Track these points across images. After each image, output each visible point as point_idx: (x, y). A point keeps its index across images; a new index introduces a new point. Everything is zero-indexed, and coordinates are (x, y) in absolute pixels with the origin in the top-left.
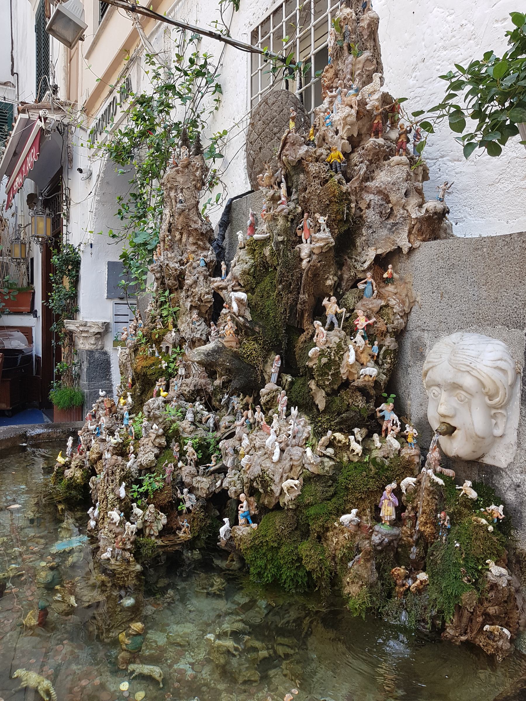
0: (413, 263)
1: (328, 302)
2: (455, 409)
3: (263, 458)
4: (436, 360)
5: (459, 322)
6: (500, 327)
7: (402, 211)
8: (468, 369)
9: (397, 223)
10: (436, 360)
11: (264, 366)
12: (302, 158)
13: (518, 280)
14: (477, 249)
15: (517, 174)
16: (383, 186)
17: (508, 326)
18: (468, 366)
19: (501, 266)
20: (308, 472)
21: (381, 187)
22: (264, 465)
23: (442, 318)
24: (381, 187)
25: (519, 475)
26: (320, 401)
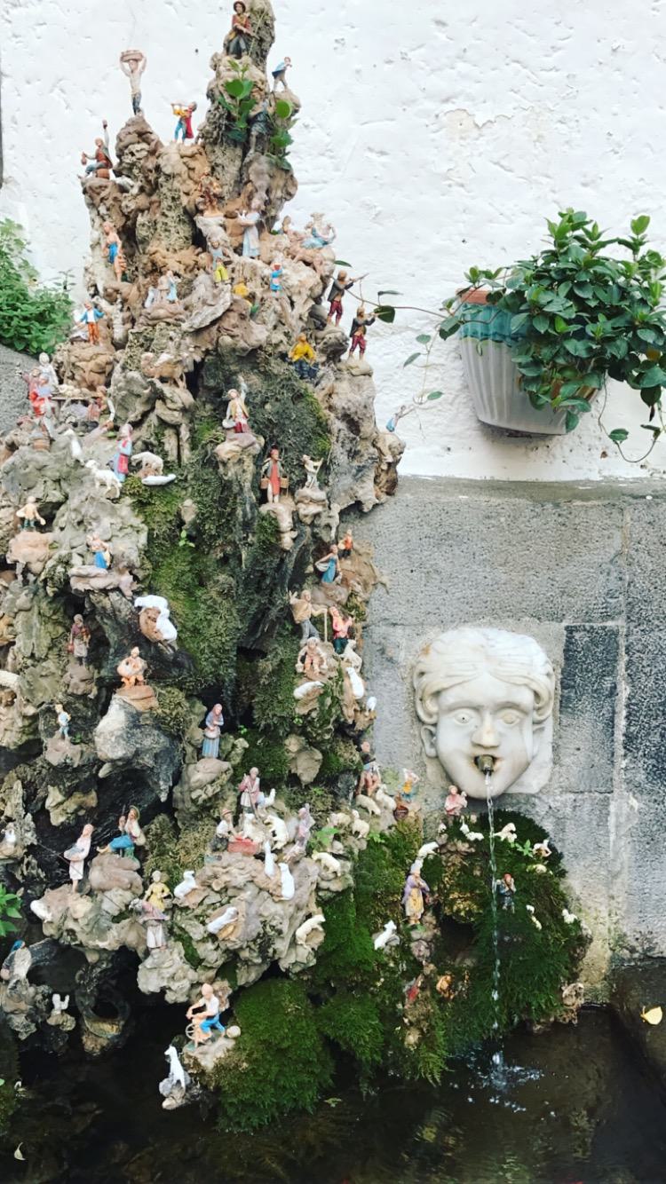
0: (372, 526)
1: (297, 600)
2: (501, 735)
3: (257, 901)
4: (469, 673)
5: (461, 614)
6: (527, 619)
7: (372, 450)
8: (526, 681)
9: (364, 467)
10: (469, 673)
11: (433, 745)
12: (260, 347)
13: (554, 563)
14: (488, 517)
15: (409, 386)
16: (353, 410)
17: (539, 619)
18: (525, 677)
19: (528, 543)
20: (329, 894)
21: (349, 409)
22: (266, 914)
23: (431, 608)
24: (349, 409)
25: (558, 798)
26: (305, 770)
